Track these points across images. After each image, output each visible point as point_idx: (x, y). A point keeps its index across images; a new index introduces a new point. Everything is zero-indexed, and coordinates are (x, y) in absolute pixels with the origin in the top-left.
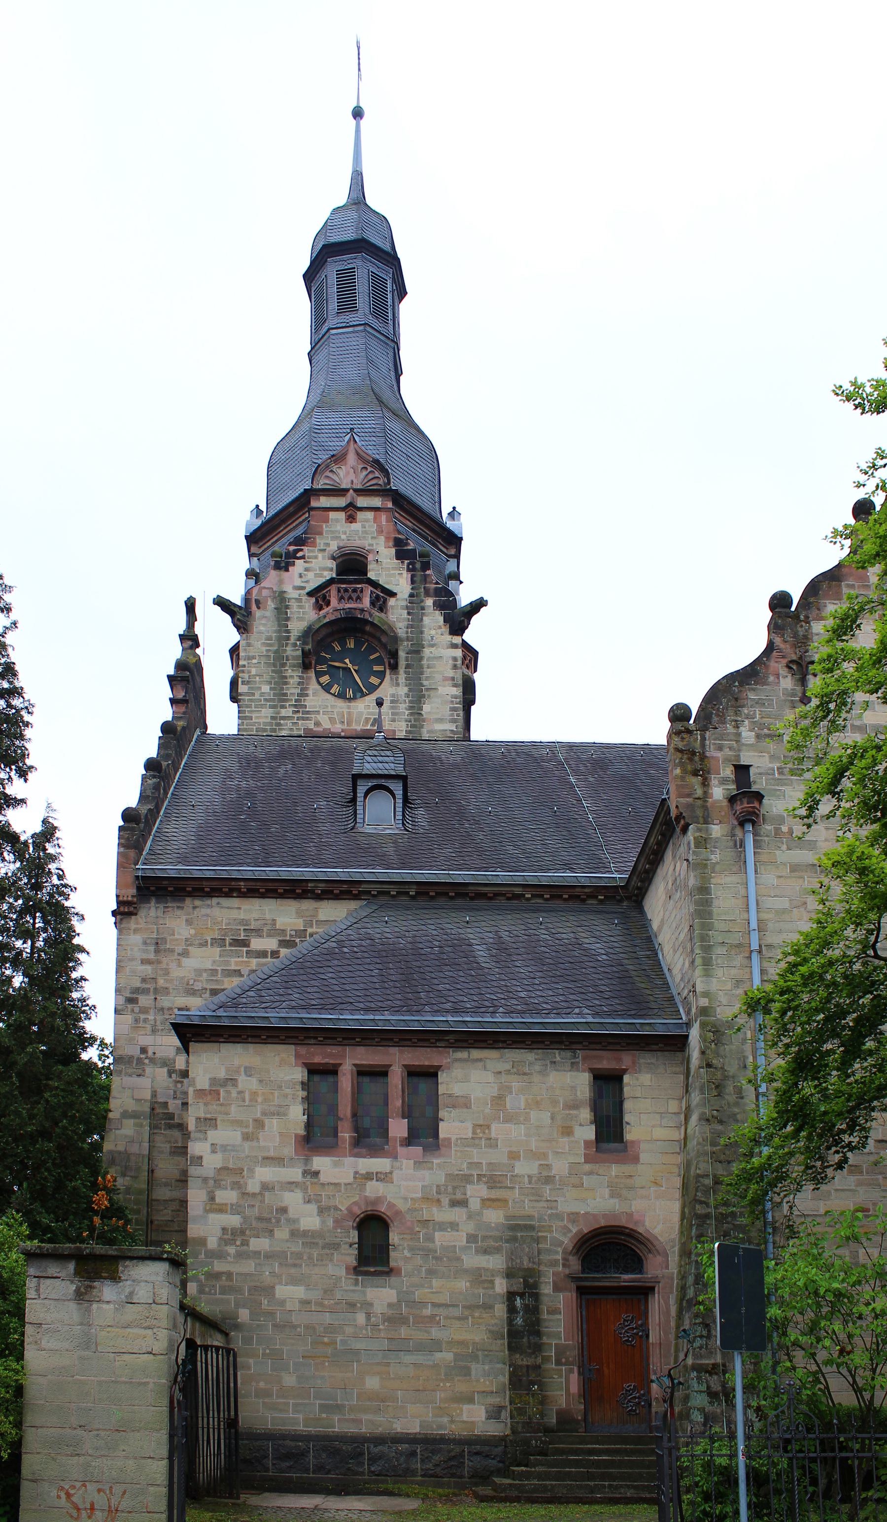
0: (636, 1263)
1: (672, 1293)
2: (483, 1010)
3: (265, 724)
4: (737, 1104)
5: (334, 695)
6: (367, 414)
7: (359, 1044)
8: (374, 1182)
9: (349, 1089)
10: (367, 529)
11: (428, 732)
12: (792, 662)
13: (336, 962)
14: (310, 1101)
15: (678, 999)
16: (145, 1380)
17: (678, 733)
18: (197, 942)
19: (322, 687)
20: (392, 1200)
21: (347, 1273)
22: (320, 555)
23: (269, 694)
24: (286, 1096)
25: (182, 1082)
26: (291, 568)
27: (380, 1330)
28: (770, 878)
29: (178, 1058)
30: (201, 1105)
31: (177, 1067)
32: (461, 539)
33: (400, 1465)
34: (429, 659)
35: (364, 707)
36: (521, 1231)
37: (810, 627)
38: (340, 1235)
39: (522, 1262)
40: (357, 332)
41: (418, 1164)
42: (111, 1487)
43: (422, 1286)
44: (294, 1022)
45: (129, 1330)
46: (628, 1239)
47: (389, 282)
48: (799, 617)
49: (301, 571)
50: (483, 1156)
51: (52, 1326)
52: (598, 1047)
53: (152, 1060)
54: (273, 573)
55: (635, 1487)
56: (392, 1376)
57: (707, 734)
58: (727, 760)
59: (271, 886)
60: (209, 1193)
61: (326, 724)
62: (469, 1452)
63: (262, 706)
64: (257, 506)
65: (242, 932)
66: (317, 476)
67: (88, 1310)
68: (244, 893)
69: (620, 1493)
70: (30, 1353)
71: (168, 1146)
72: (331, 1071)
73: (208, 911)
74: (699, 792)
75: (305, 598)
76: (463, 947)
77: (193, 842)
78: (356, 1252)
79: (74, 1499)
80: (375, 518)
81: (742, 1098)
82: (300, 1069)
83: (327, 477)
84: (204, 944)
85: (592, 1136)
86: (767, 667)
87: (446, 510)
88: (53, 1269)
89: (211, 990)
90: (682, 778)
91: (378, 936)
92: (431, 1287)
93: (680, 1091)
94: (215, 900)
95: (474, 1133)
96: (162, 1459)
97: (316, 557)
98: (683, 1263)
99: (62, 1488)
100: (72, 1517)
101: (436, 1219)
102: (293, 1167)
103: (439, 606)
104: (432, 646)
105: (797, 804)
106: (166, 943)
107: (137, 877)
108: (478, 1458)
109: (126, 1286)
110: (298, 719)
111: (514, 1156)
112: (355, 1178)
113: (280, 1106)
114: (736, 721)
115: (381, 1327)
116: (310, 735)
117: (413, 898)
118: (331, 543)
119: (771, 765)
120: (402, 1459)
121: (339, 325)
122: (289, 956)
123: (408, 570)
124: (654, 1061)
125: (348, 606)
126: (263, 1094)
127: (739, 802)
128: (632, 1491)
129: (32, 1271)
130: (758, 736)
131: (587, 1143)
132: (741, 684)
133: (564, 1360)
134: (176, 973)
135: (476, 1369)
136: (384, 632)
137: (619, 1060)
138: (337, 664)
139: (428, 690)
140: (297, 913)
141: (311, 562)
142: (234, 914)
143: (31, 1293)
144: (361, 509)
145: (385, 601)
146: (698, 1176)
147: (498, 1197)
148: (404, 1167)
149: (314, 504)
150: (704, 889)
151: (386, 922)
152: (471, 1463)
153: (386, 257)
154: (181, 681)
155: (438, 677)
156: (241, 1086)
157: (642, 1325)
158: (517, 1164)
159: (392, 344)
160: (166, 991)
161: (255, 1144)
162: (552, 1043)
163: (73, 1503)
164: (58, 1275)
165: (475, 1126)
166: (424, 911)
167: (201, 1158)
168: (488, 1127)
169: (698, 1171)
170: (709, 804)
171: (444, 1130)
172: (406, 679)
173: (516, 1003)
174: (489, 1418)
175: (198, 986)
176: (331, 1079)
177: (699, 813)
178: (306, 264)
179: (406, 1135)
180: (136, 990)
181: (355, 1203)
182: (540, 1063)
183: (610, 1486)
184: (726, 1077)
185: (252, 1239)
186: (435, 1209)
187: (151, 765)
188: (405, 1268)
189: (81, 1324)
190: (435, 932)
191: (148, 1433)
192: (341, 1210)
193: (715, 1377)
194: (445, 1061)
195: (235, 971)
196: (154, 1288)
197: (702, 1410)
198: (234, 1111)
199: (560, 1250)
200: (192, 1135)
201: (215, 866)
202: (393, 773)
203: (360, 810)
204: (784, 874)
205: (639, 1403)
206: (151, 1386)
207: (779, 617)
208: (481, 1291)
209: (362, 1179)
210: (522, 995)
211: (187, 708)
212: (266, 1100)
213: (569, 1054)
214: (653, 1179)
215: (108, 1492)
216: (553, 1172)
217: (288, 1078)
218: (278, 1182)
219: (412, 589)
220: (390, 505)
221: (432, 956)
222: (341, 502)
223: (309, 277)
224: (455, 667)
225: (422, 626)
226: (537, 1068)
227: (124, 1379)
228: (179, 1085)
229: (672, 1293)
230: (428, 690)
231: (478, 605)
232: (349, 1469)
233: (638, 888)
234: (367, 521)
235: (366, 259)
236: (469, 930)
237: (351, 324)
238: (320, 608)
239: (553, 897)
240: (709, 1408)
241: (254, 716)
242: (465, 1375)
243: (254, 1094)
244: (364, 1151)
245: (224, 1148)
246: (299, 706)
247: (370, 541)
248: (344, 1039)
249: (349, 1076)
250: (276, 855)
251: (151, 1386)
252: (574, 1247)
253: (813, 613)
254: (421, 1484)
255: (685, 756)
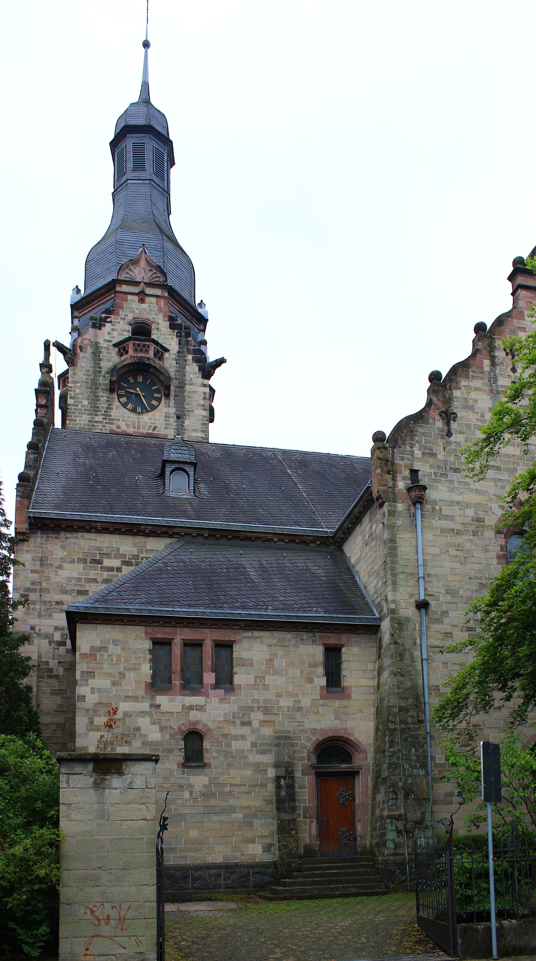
0: (347, 757)
1: (369, 774)
2: (259, 607)
3: (85, 425)
4: (411, 665)
5: (129, 410)
6: (153, 236)
7: (185, 627)
8: (195, 711)
9: (179, 654)
10: (152, 308)
11: (188, 437)
12: (442, 412)
13: (164, 576)
14: (154, 661)
15: (371, 604)
16: (141, 837)
17: (379, 448)
18: (68, 560)
19: (122, 404)
20: (206, 722)
21: (178, 767)
22: (122, 322)
23: (87, 406)
24: (139, 658)
25: (58, 649)
26: (103, 328)
27: (198, 801)
28: (429, 536)
29: (55, 633)
30: (85, 663)
31: (55, 639)
32: (207, 320)
33: (212, 882)
34: (189, 392)
35: (146, 418)
36: (284, 740)
37: (452, 393)
38: (173, 744)
39: (284, 758)
40: (145, 184)
41: (221, 700)
42: (120, 905)
43: (224, 774)
44: (145, 612)
45: (130, 806)
46: (344, 744)
47: (166, 155)
48: (446, 386)
49: (110, 330)
50: (261, 696)
51: (78, 805)
52: (329, 631)
53: (38, 635)
54: (91, 330)
55: (356, 887)
56: (206, 829)
57: (395, 450)
58: (406, 466)
59: (117, 526)
60: (89, 718)
61: (124, 428)
62: (253, 872)
63: (83, 413)
64: (77, 286)
65: (98, 555)
66: (121, 272)
67: (103, 794)
68: (100, 530)
69: (348, 891)
70: (63, 823)
71: (49, 689)
72: (167, 643)
73: (76, 541)
74: (391, 484)
75: (111, 348)
76: (240, 569)
77: (62, 496)
78: (183, 754)
79: (96, 914)
80: (157, 302)
81: (414, 662)
82: (148, 641)
83: (127, 273)
84: (73, 562)
85: (324, 683)
86: (429, 414)
87: (198, 301)
88: (78, 768)
89: (77, 591)
90: (381, 475)
91: (188, 560)
92: (229, 774)
93: (374, 658)
94: (80, 534)
95: (255, 681)
96: (154, 885)
97: (119, 323)
98: (378, 757)
99: (88, 908)
100: (95, 925)
101: (233, 733)
102: (144, 702)
103: (195, 360)
104: (191, 384)
105: (507, 495)
106: (48, 560)
107: (30, 517)
108: (258, 875)
109: (128, 778)
110: (106, 423)
111: (279, 695)
112: (183, 709)
113: (135, 664)
114: (411, 444)
115: (199, 799)
116: (113, 432)
117: (206, 538)
118: (129, 314)
119: (430, 471)
120: (213, 879)
121: (133, 178)
122: (134, 571)
123: (177, 336)
124: (359, 640)
125: (140, 355)
126: (125, 656)
127: (413, 491)
128: (355, 889)
129: (63, 770)
130: (423, 454)
131: (321, 687)
132: (414, 423)
133: (308, 816)
134: (54, 579)
135: (256, 822)
136: (162, 373)
137: (340, 639)
138: (131, 391)
139: (188, 411)
140: (133, 544)
141: (116, 325)
142: (93, 544)
143: (63, 785)
144: (148, 295)
145: (162, 354)
146: (389, 707)
147: (270, 720)
148: (213, 702)
149: (118, 289)
150: (393, 541)
151: (192, 552)
152: (254, 879)
153: (165, 140)
154: (44, 393)
155: (194, 404)
156: (110, 651)
157: (351, 794)
158: (281, 700)
159: (167, 195)
160: (48, 590)
161: (119, 688)
162: (302, 628)
163: (95, 916)
164: (82, 772)
165: (256, 677)
166: (214, 546)
167: (84, 696)
168: (264, 678)
169: (390, 704)
170: (396, 491)
171: (237, 679)
172: (174, 403)
173: (278, 603)
174: (264, 851)
175: (69, 588)
176: (166, 648)
177: (391, 496)
178: (112, 137)
179: (214, 682)
180: (28, 590)
181: (183, 724)
182: (294, 640)
183: (343, 887)
184: (405, 650)
185: (118, 747)
186: (232, 728)
187: (31, 446)
188: (214, 763)
189: (98, 803)
190: (222, 560)
191: (144, 870)
192: (174, 729)
193: (400, 822)
194: (238, 638)
195: (93, 579)
196: (146, 778)
197: (393, 841)
198: (106, 667)
199: (306, 751)
200: (79, 682)
201: (80, 512)
202: (188, 461)
203: (167, 481)
204: (437, 534)
205: (350, 839)
206: (145, 840)
207: (435, 386)
208: (259, 776)
209: (187, 709)
210: (281, 599)
211: (47, 411)
212: (126, 661)
213: (311, 635)
214: (359, 709)
215: (118, 908)
216: (302, 705)
217: (140, 647)
218: (134, 711)
219: (179, 348)
220: (166, 295)
221: (223, 574)
222: (136, 290)
223: (114, 145)
224: (205, 398)
225: (185, 372)
226: (293, 643)
227: (127, 837)
228: (56, 651)
229: (369, 774)
230: (188, 411)
231: (220, 362)
232: (180, 886)
233: (341, 538)
234: (152, 303)
235: (152, 138)
236: (243, 559)
237: (142, 178)
238: (122, 355)
239: (290, 541)
240: (397, 840)
241: (77, 419)
242: (250, 827)
243: (118, 657)
244: (188, 692)
245: (100, 690)
246: (106, 415)
247: (154, 316)
248: (176, 623)
249: (179, 646)
250: (117, 507)
251: (145, 840)
252: (314, 749)
253: (454, 385)
254: (224, 893)
255: (383, 462)
